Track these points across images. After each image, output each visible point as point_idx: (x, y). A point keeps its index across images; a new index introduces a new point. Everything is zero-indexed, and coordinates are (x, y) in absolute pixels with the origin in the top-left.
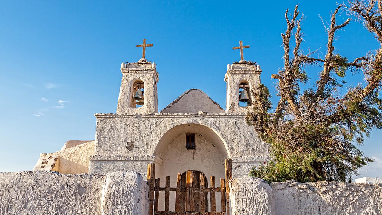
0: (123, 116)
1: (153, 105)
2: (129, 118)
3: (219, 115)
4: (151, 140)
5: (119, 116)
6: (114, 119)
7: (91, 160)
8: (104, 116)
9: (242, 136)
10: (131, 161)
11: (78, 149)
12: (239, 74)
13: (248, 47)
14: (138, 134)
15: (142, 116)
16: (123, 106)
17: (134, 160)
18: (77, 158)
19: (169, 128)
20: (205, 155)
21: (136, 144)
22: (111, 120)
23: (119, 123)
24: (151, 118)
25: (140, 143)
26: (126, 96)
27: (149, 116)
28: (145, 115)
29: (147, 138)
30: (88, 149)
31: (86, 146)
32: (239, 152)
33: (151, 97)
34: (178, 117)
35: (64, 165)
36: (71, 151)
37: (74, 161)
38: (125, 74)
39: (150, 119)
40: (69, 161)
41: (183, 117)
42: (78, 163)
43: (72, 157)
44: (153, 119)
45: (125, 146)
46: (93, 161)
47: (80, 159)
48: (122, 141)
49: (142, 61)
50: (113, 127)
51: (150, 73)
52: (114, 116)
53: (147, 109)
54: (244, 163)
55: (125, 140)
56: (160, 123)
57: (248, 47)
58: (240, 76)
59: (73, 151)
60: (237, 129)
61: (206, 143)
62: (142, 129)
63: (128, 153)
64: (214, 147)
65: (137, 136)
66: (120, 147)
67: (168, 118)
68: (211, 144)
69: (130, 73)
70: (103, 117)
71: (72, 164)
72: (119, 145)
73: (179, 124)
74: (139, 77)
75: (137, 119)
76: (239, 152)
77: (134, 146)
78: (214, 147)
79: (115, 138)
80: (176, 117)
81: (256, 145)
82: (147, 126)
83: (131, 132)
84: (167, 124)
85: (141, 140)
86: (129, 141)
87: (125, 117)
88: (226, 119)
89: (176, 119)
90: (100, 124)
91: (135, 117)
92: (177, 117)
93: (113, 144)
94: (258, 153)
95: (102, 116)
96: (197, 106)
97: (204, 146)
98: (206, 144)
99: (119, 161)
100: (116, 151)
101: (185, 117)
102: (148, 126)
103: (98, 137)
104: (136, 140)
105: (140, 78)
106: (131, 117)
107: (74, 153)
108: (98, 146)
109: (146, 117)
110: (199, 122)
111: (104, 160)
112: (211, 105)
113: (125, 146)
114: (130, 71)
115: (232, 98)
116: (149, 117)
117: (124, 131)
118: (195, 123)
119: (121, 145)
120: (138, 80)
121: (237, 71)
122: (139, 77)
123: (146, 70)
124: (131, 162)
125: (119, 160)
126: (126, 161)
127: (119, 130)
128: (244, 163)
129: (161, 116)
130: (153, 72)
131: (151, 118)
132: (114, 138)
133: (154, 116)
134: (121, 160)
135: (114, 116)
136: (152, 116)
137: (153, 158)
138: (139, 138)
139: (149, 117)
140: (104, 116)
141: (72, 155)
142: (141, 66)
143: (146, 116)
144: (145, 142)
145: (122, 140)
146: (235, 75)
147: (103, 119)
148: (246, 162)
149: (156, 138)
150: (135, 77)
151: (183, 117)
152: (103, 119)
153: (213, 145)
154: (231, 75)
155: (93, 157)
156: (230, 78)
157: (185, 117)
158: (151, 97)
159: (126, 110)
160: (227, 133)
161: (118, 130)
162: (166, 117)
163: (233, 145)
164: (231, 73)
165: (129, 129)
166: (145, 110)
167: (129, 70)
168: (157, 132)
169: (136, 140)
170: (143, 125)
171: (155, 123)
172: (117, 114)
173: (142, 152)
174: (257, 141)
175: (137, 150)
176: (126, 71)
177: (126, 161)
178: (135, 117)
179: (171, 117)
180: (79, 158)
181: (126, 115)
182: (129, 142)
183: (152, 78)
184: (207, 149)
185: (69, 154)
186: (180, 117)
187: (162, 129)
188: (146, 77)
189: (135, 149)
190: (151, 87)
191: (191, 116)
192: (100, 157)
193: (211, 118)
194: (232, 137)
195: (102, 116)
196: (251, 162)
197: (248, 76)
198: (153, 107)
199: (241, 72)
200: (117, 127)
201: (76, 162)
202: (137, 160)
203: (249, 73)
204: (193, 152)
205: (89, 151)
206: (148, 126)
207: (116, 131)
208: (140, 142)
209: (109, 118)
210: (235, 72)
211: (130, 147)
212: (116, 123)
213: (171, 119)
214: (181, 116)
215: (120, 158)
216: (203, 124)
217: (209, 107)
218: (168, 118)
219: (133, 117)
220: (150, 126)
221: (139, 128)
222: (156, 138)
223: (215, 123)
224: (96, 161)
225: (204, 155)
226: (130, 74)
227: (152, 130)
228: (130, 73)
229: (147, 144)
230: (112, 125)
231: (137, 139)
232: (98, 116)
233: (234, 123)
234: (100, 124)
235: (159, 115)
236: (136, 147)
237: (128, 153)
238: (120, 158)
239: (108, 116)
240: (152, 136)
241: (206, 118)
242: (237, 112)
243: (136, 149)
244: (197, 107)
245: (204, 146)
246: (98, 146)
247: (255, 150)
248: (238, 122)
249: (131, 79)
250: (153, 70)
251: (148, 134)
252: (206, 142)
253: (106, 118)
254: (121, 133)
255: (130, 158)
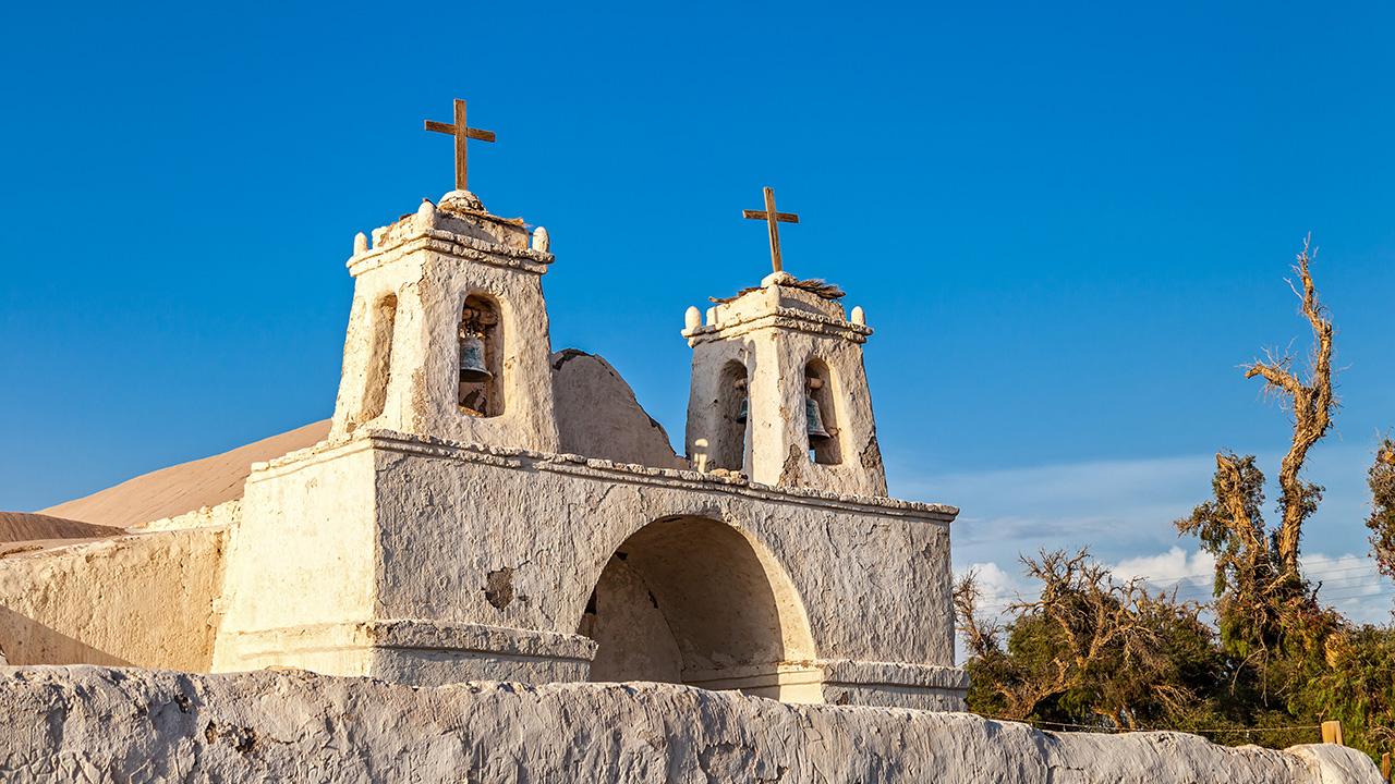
0: (474, 455)
1: (550, 418)
2: (494, 464)
3: (680, 478)
4: (572, 572)
5: (459, 451)
6: (438, 464)
7: (381, 643)
8: (404, 447)
9: (846, 582)
10: (517, 658)
11: (77, 567)
12: (805, 332)
13: (489, 138)
14: (528, 541)
15: (541, 465)
16: (438, 405)
17: (934, 687)
18: (77, 613)
19: (632, 525)
20: (627, 638)
21: (520, 583)
22: (426, 467)
23: (458, 483)
24: (570, 474)
25: (533, 581)
26: (448, 360)
27: (565, 467)
28: (553, 463)
29: (558, 559)
30: (131, 574)
31: (120, 557)
32: (841, 642)
33: (542, 382)
34: (660, 486)
35: (14, 644)
36: (46, 575)
37: (60, 628)
38: (436, 255)
39: (566, 478)
40: (36, 625)
41: (677, 487)
42: (83, 640)
43: (50, 603)
44: (575, 480)
45: (483, 589)
46: (385, 647)
47: (91, 617)
48: (471, 566)
49: (470, 205)
50: (436, 500)
51: (530, 271)
52: (441, 451)
53: (531, 432)
54: (860, 685)
55: (480, 562)
56: (601, 500)
57: (489, 138)
58: (807, 340)
59: (54, 576)
60: (833, 556)
61: (630, 587)
62: (539, 518)
63: (493, 619)
64: (656, 606)
65: (521, 549)
66: (463, 591)
67: (629, 482)
68: (646, 593)
69: (458, 256)
70: (400, 451)
71: (52, 642)
72: (460, 583)
73: (664, 514)
74: (488, 282)
75: (521, 473)
76: (841, 642)
77: (511, 590)
78: (656, 606)
79: (444, 550)
80: (653, 481)
81: (883, 623)
82: (558, 510)
83: (501, 530)
84: (623, 508)
85: (537, 568)
86: (496, 567)
87: (481, 458)
88: (801, 509)
89: (653, 492)
90: (386, 481)
91: (517, 463)
92: (658, 482)
93: (438, 573)
94: (889, 651)
95: (395, 446)
96: (596, 427)
97: (626, 601)
98: (631, 594)
99: (477, 655)
100: (451, 609)
101: (680, 487)
102: (562, 509)
103: (382, 540)
104: (520, 567)
105: (494, 285)
106: (501, 461)
107: (61, 589)
108: (386, 578)
109: (552, 471)
110: (724, 511)
111: (428, 644)
112: (641, 430)
113: (483, 589)
114: (456, 249)
115: (791, 425)
116: (563, 473)
117: (475, 522)
118: (710, 515)
119: (467, 581)
120: (480, 292)
121: (801, 319)
122: (488, 282)
123: (517, 258)
124: (518, 662)
125: (478, 651)
126: (504, 654)
127: (458, 515)
128: (860, 685)
129: (605, 474)
130: (543, 268)
131: (570, 474)
132: (440, 548)
133: (583, 470)
134: (488, 653)
135: (441, 451)
136: (574, 469)
137: (590, 647)
138: (529, 558)
139: (563, 473)
140: (404, 447)
141: (51, 595)
142: (489, 230)
143: (556, 467)
144: (549, 576)
145: (469, 560)
146: (793, 334)
147: (399, 456)
148: (867, 685)
149: (589, 562)
150: (472, 279)
151: (677, 487)
152: (399, 456)
153: (653, 599)
154: (780, 331)
155: (390, 629)
156: (778, 342)
157: (685, 485)
158: (542, 382)
159: (453, 426)
160: (806, 568)
161: (453, 514)
162: (623, 481)
163: (822, 614)
164: (782, 324)
165: (494, 514)
166: (523, 433)
167: (455, 242)
168: (593, 539)
169: (520, 567)
170: (542, 504)
171: (583, 497)
172: (454, 442)
173: (541, 619)
174: (885, 607)
175: (523, 609)
176: (442, 245)
177: (504, 654)
178: (517, 463)
179: (637, 479)
180: (86, 617)
181: (487, 451)
182: (493, 572)
183: (537, 296)
184: (632, 615)
185: (34, 588)
186: (667, 486)
187: (608, 529)
188: (517, 289)
189: (515, 602)
190: (538, 333)
191: (700, 486)
192: (415, 633)
193: (757, 502)
194: (820, 583)
195: (395, 446)
196: (879, 684)
197: (829, 342)
198: (551, 423)
199: (812, 326)
200: (450, 500)
201: (72, 634)
202: (540, 656)
203: (833, 335)
204: (590, 622)
205: (134, 584)
206: (562, 509)
207: (445, 517)
208: (532, 575)
209: (422, 454)
210: (794, 324)
211: (499, 593)
212: (446, 482)
213: (637, 487)
214: (671, 483)
215: (485, 643)
216: (735, 524)
217: (636, 436)
218: (629, 482)
219: (511, 463)
220: (566, 509)
221: (528, 515)
222: (589, 562)
223: (769, 521)
224: (402, 647)
225: (622, 639)
226: (454, 261)
227: (574, 527)
228: (458, 256)
229: (559, 586)
230: (432, 488)
231: (522, 560)
232: (381, 444)
233: (824, 528)
234: (386, 481)
235: (600, 469)
236: (520, 598)
237: (493, 619)
238: (485, 643)
239: (419, 449)
240: (575, 555)
241: (744, 500)
242: (807, 484)
243: (520, 605)
244: (597, 430)
245: (626, 601)
246: (386, 578)
247: (881, 638)
248: (835, 527)
249: (458, 284)
250: (541, 263)
251: (560, 543)
252: (632, 583)
253: (409, 453)
254: (467, 527)
255: (517, 644)
